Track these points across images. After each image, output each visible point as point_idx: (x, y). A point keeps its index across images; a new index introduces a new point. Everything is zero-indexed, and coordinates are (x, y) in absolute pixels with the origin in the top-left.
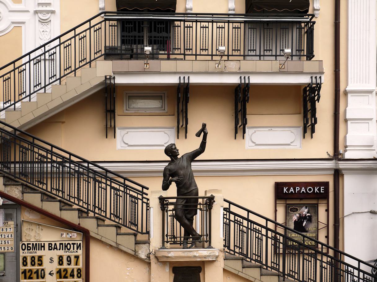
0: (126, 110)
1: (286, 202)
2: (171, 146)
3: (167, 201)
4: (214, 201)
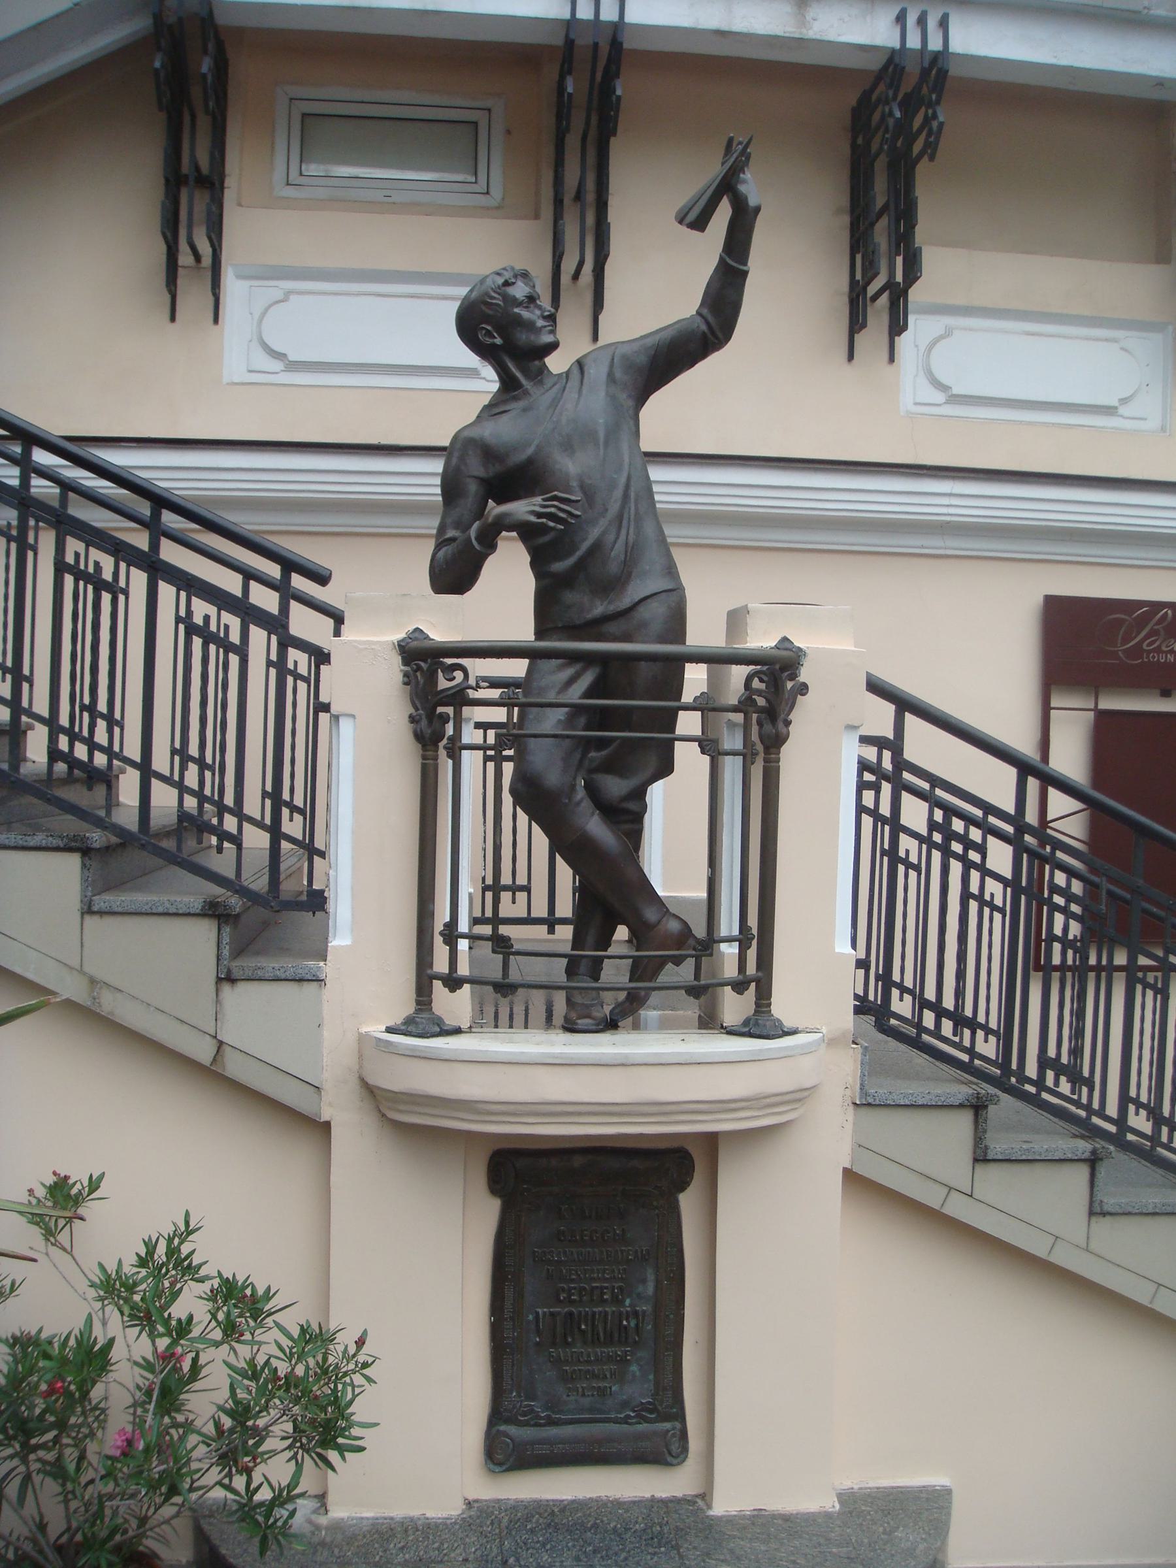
0: (288, 184)
1: (1096, 704)
2: (500, 281)
3: (459, 675)
4: (803, 689)
